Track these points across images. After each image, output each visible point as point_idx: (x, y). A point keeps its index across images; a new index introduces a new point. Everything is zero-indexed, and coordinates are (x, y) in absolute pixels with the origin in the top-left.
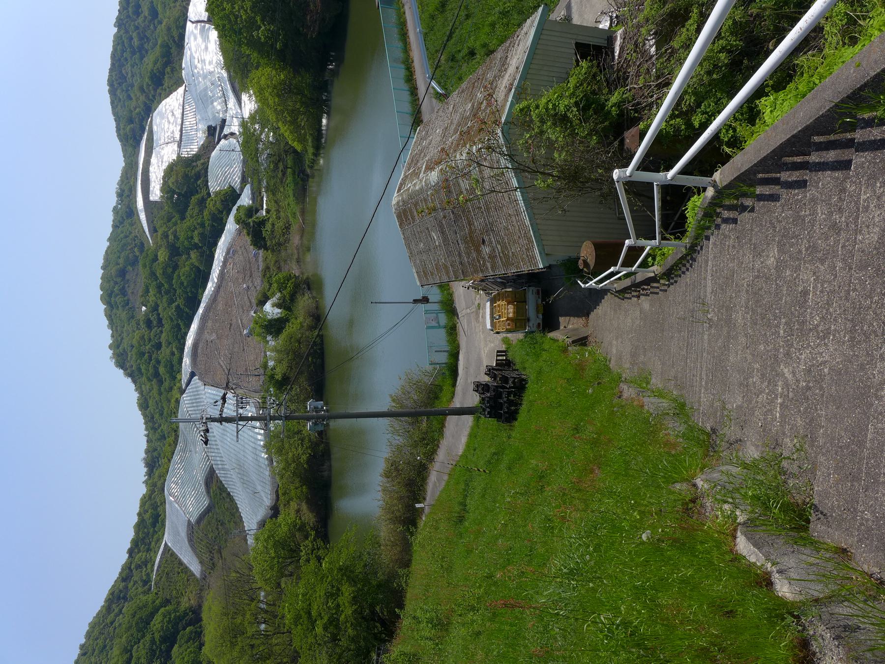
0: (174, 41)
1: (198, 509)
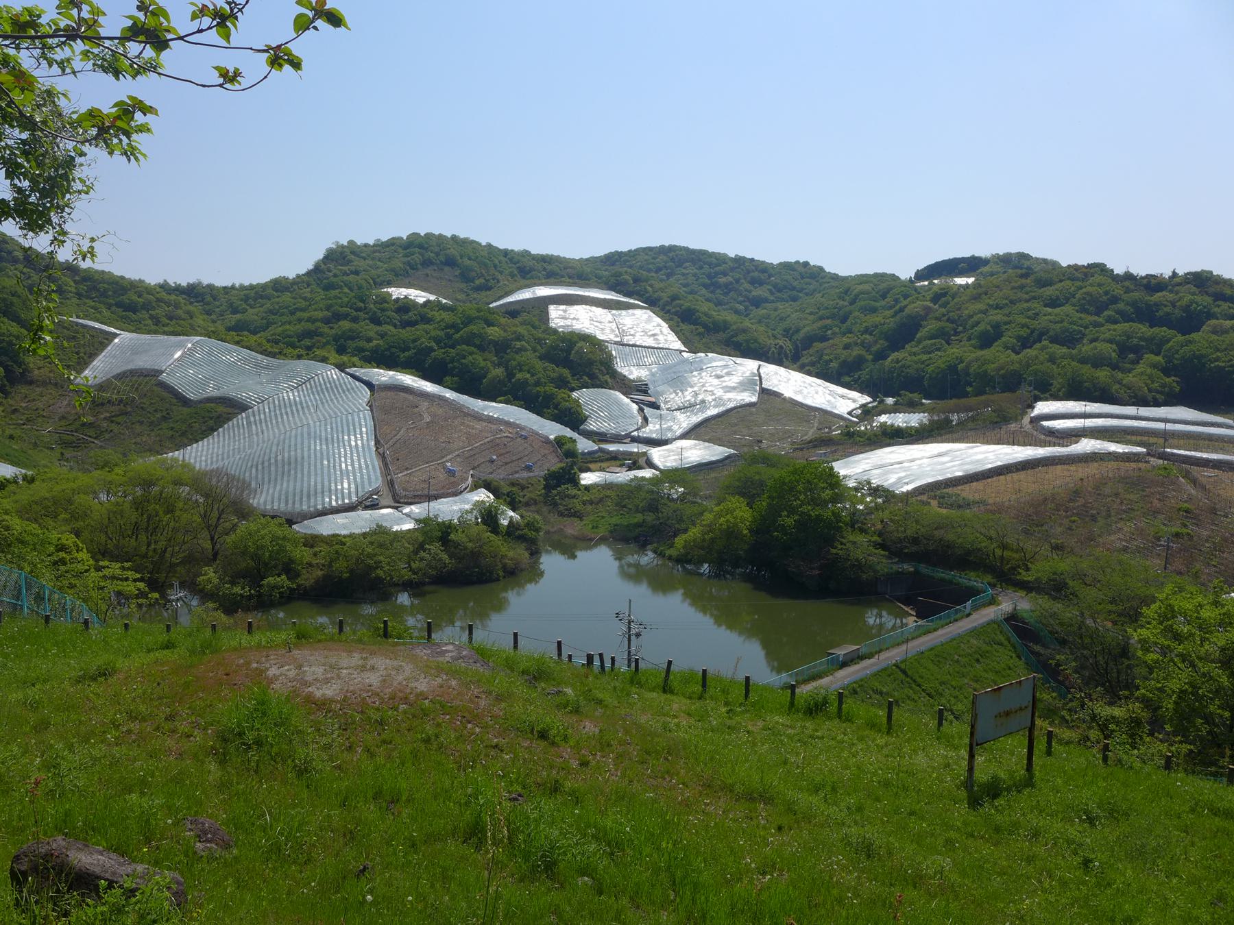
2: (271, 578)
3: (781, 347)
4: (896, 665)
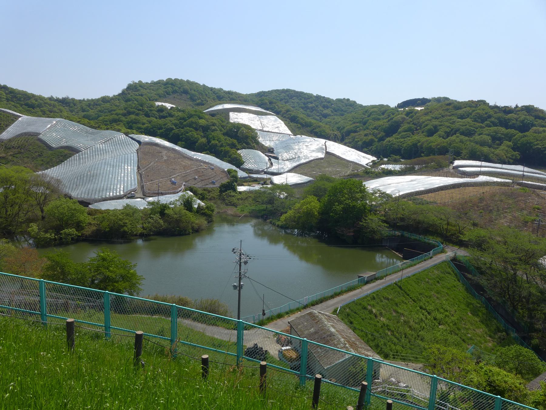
0: (314, 129)
2: (66, 230)
3: (336, 135)
4: (396, 284)
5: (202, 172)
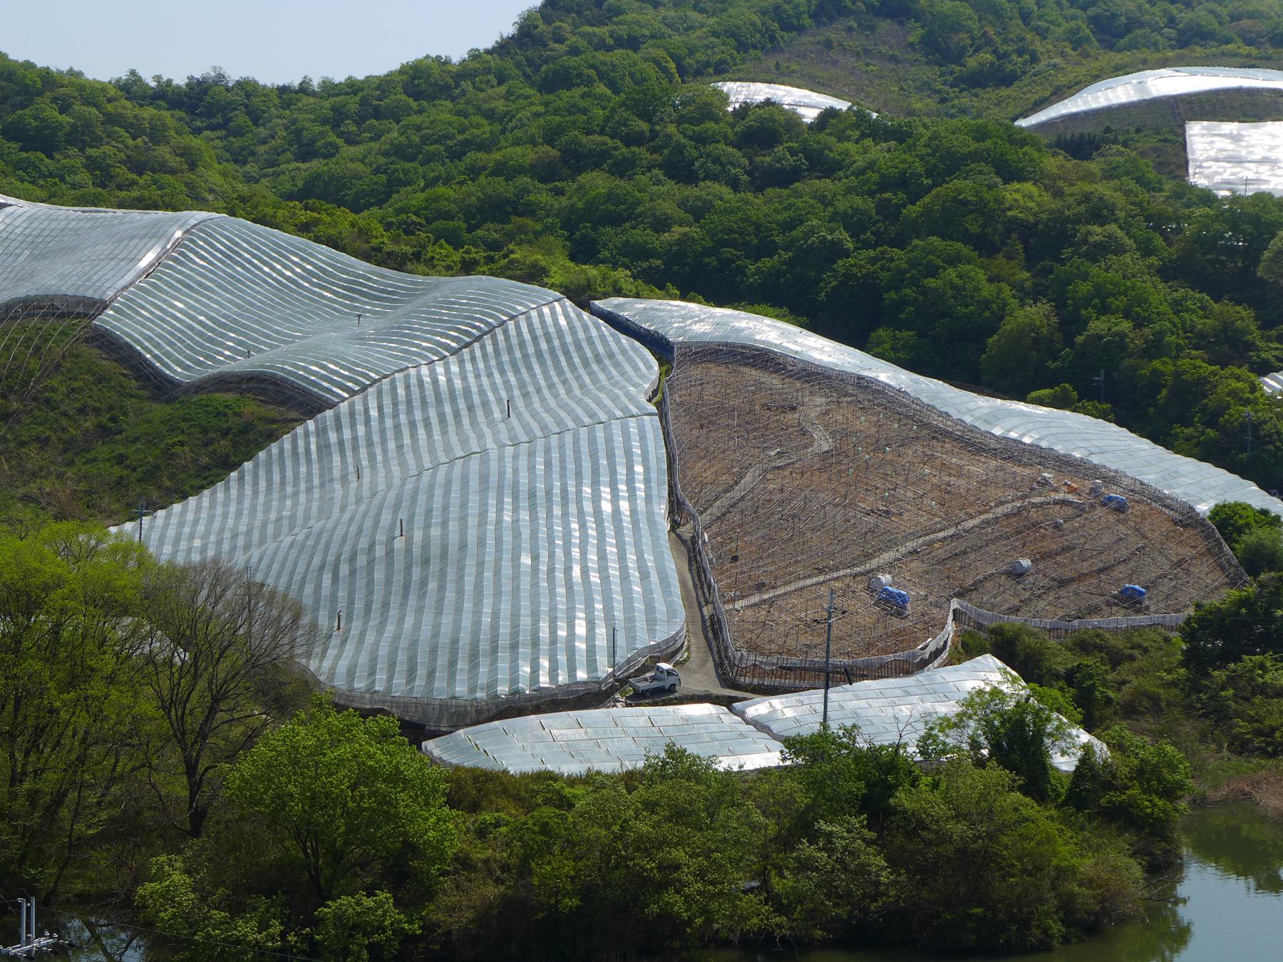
1: (149, 339)
2: (345, 900)
5: (1057, 527)
